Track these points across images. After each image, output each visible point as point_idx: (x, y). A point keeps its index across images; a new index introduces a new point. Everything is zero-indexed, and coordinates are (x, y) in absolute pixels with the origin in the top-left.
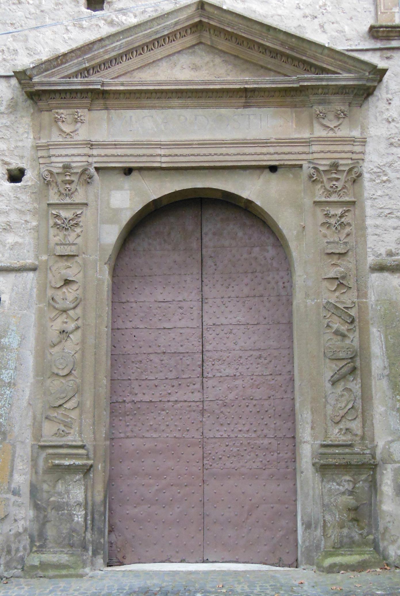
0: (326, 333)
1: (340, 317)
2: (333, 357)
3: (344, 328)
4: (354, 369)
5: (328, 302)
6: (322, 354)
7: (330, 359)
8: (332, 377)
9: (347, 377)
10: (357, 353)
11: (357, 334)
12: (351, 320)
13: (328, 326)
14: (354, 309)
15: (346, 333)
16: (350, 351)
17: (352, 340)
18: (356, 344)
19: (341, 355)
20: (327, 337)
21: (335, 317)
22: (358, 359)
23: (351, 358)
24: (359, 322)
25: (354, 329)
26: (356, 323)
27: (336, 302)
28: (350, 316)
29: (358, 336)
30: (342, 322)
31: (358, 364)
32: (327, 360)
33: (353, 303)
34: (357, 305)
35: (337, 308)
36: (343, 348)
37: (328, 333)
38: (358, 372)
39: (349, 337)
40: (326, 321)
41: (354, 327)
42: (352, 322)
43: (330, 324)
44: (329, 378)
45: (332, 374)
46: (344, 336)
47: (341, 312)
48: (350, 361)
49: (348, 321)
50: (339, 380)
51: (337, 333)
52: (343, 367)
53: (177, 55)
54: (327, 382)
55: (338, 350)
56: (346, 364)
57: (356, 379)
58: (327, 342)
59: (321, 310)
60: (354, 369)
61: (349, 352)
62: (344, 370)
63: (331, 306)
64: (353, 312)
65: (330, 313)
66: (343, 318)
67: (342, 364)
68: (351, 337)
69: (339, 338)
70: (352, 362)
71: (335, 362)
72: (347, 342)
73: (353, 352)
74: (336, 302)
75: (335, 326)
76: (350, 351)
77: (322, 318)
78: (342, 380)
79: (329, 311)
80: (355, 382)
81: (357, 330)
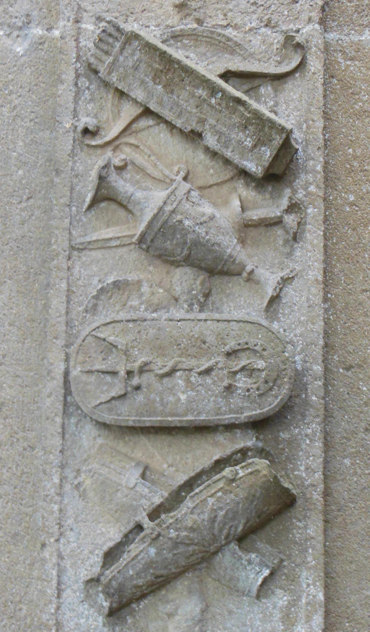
0: (82, 248)
1: (194, 136)
2: (126, 414)
3: (218, 214)
4: (276, 506)
5: (114, 37)
6: (51, 401)
7: (104, 426)
8: (111, 556)
9: (225, 559)
10: (299, 381)
11: (309, 257)
12: (267, 153)
13: (104, 196)
14: (294, 92)
15: (230, 245)
16: (249, 371)
17: (275, 300)
18: (301, 324)
19: (184, 399)
20: (94, 272)
21: (156, 137)
22: (307, 437)
23: (259, 425)
24: (329, 179)
25: (290, 220)
26: (308, 183)
27: (176, 37)
28: (261, 126)
29: (315, 273)
30: (210, 172)
31: (306, 470)
32: (89, 438)
33: (292, 44)
34: (315, 64)
35: (170, 71)
36: (201, 346)
37: (104, 245)
38: (308, 527)
39: (250, 278)
40: (91, 165)
41: (293, 207)
42: (278, 174)
43: (123, 185)
44: (93, 565)
45: (113, 535)
46: (216, 269)
47: (201, 103)
48: (249, 441)
49: (254, 167)
50: (160, 583)
51: (167, 244)
52: (189, 485)
53: (215, 187)
54: (72, 595)
55: (162, 365)
56: (219, 465)
57: (293, 579)
58: (93, 309)
59: (65, 92)
60: (276, 506)
61: (242, 382)
62: (191, 513)
63: (133, 56)
64: (292, 109)
65: (129, 111)
66: (211, 140)
67: (179, 462)
68: (270, 279)
69: (183, 280)
70: (262, 453)
71: (147, 450)
72: (240, 306)
73: (273, 382)
74: (176, 37)
75: (151, 199)
76: (249, 371)
77: (67, 143)
78: (181, 586)
79: (121, 94)
80: (281, 599)
81: (314, 235)
